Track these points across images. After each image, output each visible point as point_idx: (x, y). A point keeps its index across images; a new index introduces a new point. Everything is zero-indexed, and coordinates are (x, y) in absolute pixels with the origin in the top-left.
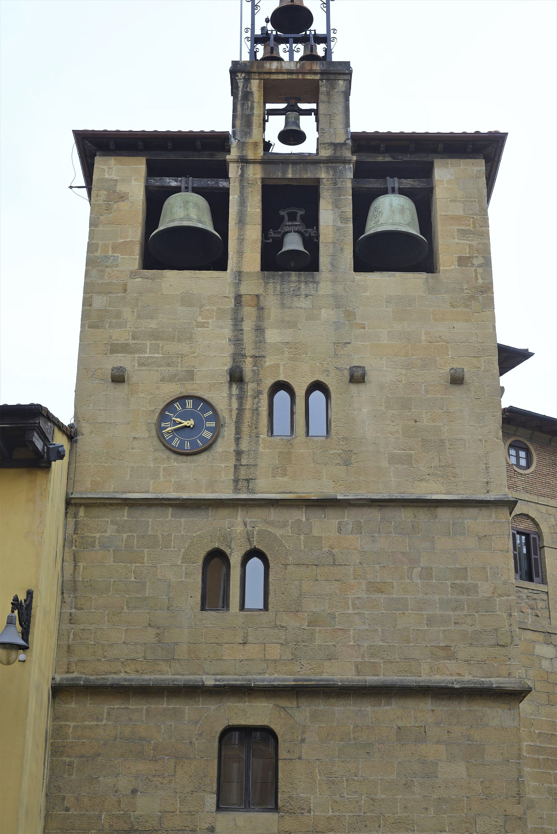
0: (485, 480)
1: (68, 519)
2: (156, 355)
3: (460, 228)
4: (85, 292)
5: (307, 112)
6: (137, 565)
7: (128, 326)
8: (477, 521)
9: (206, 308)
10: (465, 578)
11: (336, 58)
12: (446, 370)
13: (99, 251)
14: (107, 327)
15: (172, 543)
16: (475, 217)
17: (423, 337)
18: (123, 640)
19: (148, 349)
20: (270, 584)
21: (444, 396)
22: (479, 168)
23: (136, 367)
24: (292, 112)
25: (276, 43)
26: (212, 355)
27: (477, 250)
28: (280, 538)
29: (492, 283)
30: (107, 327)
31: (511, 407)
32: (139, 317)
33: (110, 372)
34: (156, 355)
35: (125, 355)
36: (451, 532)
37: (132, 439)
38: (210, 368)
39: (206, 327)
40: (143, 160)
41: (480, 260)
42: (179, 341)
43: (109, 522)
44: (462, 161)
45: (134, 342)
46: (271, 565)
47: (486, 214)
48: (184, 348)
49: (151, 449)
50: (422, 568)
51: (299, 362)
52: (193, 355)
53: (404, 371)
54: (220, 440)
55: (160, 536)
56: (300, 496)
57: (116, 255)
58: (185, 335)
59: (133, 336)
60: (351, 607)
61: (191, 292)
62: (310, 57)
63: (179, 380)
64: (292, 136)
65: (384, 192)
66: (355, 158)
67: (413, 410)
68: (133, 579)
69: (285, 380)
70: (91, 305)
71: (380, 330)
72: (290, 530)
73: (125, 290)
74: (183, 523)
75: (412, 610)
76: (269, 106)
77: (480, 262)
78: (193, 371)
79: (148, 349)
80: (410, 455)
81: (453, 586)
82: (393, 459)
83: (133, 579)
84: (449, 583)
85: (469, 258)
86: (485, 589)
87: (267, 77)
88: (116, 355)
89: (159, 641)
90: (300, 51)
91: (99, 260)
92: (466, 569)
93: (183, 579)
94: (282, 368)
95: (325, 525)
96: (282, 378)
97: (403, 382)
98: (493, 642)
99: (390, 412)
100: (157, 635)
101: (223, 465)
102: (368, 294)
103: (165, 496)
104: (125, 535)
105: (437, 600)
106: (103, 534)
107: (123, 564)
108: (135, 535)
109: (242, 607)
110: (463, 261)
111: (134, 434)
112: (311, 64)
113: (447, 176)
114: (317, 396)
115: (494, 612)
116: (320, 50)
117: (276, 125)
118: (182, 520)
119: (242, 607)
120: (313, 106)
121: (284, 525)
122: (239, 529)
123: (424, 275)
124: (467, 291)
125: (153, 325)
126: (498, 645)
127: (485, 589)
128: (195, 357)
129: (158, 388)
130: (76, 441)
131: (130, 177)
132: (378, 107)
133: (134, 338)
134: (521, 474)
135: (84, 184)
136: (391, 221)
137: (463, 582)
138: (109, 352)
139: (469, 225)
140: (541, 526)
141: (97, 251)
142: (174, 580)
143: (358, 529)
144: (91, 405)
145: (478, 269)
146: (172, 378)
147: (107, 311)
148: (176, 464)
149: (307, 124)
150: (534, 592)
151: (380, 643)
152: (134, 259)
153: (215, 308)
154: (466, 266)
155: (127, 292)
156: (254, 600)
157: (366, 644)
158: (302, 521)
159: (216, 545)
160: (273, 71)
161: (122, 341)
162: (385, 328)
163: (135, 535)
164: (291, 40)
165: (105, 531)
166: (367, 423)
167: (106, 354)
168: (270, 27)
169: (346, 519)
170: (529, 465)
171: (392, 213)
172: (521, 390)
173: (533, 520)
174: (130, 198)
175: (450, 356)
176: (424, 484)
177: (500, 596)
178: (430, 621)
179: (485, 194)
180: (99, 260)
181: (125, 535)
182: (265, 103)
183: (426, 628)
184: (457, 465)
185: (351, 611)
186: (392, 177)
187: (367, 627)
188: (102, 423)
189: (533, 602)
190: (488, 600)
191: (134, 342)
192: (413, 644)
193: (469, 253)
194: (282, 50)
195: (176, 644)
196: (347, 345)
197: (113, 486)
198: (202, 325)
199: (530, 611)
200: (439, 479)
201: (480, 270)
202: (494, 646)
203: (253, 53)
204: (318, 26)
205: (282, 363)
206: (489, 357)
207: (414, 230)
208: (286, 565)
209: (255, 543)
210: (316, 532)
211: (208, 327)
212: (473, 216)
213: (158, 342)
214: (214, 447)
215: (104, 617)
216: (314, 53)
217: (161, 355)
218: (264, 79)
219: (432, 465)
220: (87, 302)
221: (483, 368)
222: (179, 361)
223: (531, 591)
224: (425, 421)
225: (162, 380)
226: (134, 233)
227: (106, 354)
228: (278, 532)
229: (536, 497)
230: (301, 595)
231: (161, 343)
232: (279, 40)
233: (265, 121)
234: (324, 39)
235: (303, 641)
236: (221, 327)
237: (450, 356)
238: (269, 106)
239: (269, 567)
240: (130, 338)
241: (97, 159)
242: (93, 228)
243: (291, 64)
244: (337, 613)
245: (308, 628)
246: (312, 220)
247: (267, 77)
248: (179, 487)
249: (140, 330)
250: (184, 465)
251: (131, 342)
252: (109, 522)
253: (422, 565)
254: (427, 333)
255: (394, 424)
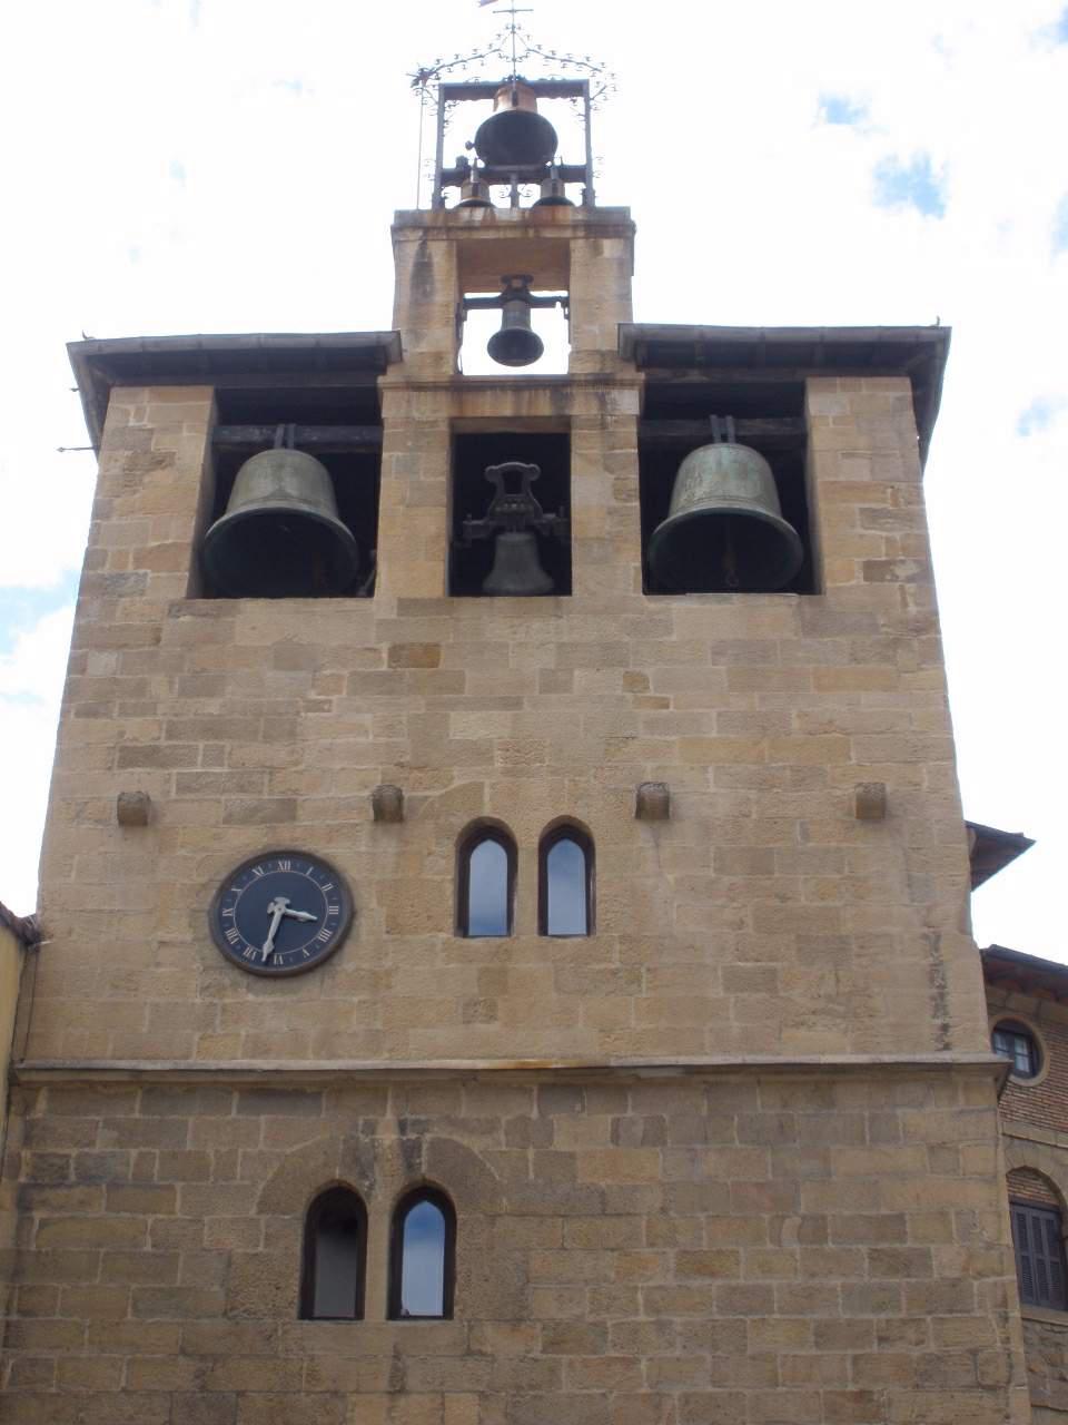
0: (939, 1022)
1: (12, 1117)
2: (217, 770)
3: (866, 506)
4: (74, 646)
5: (548, 303)
6: (161, 1216)
7: (159, 712)
8: (928, 1116)
9: (328, 672)
10: (901, 1237)
11: (599, 203)
12: (848, 791)
13: (108, 566)
14: (115, 715)
15: (239, 1169)
16: (897, 485)
17: (795, 724)
18: (123, 1384)
19: (200, 758)
20: (458, 1259)
21: (844, 845)
22: (899, 394)
23: (173, 795)
24: (516, 299)
25: (485, 182)
26: (338, 767)
27: (904, 549)
28: (480, 1157)
29: (936, 613)
30: (115, 715)
31: (994, 947)
32: (183, 693)
33: (115, 805)
34: (217, 770)
35: (148, 770)
36: (868, 1137)
37: (155, 945)
38: (331, 794)
39: (324, 711)
40: (209, 390)
41: (910, 569)
42: (268, 738)
43: (101, 1124)
44: (863, 381)
45: (171, 743)
46: (460, 1216)
47: (916, 496)
48: (279, 753)
49: (197, 965)
50: (804, 1218)
51: (524, 779)
52: (294, 769)
53: (753, 795)
54: (349, 947)
55: (212, 1155)
56: (524, 1063)
57: (141, 571)
58: (280, 726)
59: (167, 731)
60: (641, 1308)
61: (295, 640)
62: (553, 201)
63: (263, 821)
64: (516, 344)
65: (708, 440)
66: (642, 376)
67: (777, 875)
68: (148, 1248)
69: (497, 816)
70: (83, 671)
71: (700, 710)
72: (503, 1138)
73: (158, 640)
74: (263, 1127)
75: (781, 1310)
76: (468, 296)
77: (910, 572)
78: (295, 801)
79: (200, 758)
80: (773, 972)
81: (875, 1256)
82: (734, 981)
83: (148, 1248)
84: (864, 1248)
85: (889, 563)
86: (946, 1259)
87: (464, 236)
88: (130, 770)
89: (203, 1388)
90: (531, 194)
91: (108, 582)
92: (900, 1218)
93: (260, 1249)
94: (487, 790)
95: (582, 1132)
96: (487, 811)
97: (754, 816)
98: (969, 1379)
99: (726, 880)
100: (200, 1374)
101: (355, 999)
102: (674, 638)
103: (225, 1065)
104: (134, 1153)
105: (839, 1289)
106: (86, 1150)
107: (127, 1215)
108: (157, 1151)
109: (395, 1310)
110: (874, 571)
111: (161, 935)
112: (553, 212)
113: (830, 410)
114: (567, 856)
115: (968, 1312)
116: (573, 192)
117: (484, 324)
118: (263, 1118)
119: (395, 1310)
120: (564, 294)
121: (490, 1128)
122: (388, 1137)
123: (793, 598)
124: (885, 629)
125: (212, 707)
126: (979, 1385)
127: (946, 1259)
128: (301, 773)
129: (217, 837)
130: (37, 950)
131: (184, 429)
132: (686, 283)
133: (170, 736)
134: (1020, 1087)
135: (90, 444)
136: (720, 492)
137: (897, 1245)
138: (116, 764)
139: (884, 501)
140: (1064, 1193)
141: (103, 564)
142: (240, 1250)
143: (655, 1136)
144: (73, 874)
145: (907, 586)
146: (249, 817)
147: (116, 681)
148: (251, 997)
149: (549, 325)
150: (1056, 1329)
151: (710, 1389)
152: (176, 580)
153: (345, 673)
154: (883, 580)
155: (162, 643)
156: (422, 1292)
157: (677, 1392)
158: (530, 1119)
159: (337, 1173)
160: (477, 224)
161: (145, 742)
162: (713, 707)
163: (157, 1151)
164: (514, 177)
165: (91, 1144)
166: (675, 905)
167: (110, 769)
168: (472, 156)
169: (630, 1113)
170: (1034, 1071)
171: (719, 477)
172: (1015, 915)
173: (1047, 1181)
174: (177, 462)
175: (854, 761)
176: (802, 1032)
177: (980, 1275)
178: (824, 1335)
179: (919, 463)
180: (108, 582)
181: (134, 1153)
182: (461, 292)
183: (814, 1352)
184: (876, 990)
185: (642, 1318)
186: (722, 415)
187: (677, 1353)
188: (92, 911)
189: (1053, 1349)
190: (954, 1283)
191: (171, 743)
192: (784, 1389)
193: (887, 555)
194: (498, 195)
195: (241, 1394)
196: (630, 741)
197: (111, 1047)
198: (316, 706)
199: (1046, 1369)
200: (838, 1021)
201: (911, 587)
202: (969, 1388)
203: (439, 201)
204: (568, 152)
205: (487, 782)
206: (938, 763)
207: (769, 510)
208: (493, 1218)
209: (424, 1168)
210: (561, 1143)
211: (329, 711)
212: (893, 484)
213: (222, 743)
214: (335, 960)
215: (83, 1333)
216: (559, 194)
217: (226, 770)
218: (457, 240)
219: (822, 993)
220: (77, 665)
221: (925, 784)
222: (266, 780)
223: (1049, 1327)
224: (803, 898)
225: (228, 820)
226: (181, 529)
227: (110, 769)
228: (476, 1144)
229: (1051, 1134)
230: (528, 1282)
231: (227, 744)
232: (489, 177)
233: (460, 319)
234: (581, 174)
235: (532, 1387)
236: (358, 710)
237: (854, 761)
238: (468, 296)
239: (455, 1222)
240: (163, 735)
241: (115, 393)
242: (99, 521)
243: (514, 210)
244: (609, 1324)
245: (545, 1356)
246: (555, 491)
247: (464, 236)
248: (258, 1047)
249: (184, 718)
250: (269, 999)
251: (163, 743)
252: (101, 1124)
253: (802, 1210)
254: (802, 715)
255: (735, 905)
